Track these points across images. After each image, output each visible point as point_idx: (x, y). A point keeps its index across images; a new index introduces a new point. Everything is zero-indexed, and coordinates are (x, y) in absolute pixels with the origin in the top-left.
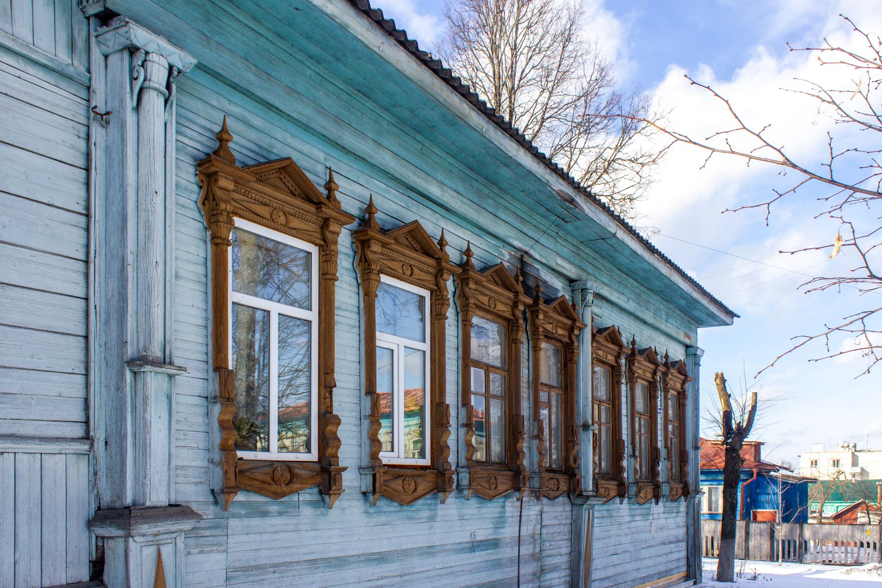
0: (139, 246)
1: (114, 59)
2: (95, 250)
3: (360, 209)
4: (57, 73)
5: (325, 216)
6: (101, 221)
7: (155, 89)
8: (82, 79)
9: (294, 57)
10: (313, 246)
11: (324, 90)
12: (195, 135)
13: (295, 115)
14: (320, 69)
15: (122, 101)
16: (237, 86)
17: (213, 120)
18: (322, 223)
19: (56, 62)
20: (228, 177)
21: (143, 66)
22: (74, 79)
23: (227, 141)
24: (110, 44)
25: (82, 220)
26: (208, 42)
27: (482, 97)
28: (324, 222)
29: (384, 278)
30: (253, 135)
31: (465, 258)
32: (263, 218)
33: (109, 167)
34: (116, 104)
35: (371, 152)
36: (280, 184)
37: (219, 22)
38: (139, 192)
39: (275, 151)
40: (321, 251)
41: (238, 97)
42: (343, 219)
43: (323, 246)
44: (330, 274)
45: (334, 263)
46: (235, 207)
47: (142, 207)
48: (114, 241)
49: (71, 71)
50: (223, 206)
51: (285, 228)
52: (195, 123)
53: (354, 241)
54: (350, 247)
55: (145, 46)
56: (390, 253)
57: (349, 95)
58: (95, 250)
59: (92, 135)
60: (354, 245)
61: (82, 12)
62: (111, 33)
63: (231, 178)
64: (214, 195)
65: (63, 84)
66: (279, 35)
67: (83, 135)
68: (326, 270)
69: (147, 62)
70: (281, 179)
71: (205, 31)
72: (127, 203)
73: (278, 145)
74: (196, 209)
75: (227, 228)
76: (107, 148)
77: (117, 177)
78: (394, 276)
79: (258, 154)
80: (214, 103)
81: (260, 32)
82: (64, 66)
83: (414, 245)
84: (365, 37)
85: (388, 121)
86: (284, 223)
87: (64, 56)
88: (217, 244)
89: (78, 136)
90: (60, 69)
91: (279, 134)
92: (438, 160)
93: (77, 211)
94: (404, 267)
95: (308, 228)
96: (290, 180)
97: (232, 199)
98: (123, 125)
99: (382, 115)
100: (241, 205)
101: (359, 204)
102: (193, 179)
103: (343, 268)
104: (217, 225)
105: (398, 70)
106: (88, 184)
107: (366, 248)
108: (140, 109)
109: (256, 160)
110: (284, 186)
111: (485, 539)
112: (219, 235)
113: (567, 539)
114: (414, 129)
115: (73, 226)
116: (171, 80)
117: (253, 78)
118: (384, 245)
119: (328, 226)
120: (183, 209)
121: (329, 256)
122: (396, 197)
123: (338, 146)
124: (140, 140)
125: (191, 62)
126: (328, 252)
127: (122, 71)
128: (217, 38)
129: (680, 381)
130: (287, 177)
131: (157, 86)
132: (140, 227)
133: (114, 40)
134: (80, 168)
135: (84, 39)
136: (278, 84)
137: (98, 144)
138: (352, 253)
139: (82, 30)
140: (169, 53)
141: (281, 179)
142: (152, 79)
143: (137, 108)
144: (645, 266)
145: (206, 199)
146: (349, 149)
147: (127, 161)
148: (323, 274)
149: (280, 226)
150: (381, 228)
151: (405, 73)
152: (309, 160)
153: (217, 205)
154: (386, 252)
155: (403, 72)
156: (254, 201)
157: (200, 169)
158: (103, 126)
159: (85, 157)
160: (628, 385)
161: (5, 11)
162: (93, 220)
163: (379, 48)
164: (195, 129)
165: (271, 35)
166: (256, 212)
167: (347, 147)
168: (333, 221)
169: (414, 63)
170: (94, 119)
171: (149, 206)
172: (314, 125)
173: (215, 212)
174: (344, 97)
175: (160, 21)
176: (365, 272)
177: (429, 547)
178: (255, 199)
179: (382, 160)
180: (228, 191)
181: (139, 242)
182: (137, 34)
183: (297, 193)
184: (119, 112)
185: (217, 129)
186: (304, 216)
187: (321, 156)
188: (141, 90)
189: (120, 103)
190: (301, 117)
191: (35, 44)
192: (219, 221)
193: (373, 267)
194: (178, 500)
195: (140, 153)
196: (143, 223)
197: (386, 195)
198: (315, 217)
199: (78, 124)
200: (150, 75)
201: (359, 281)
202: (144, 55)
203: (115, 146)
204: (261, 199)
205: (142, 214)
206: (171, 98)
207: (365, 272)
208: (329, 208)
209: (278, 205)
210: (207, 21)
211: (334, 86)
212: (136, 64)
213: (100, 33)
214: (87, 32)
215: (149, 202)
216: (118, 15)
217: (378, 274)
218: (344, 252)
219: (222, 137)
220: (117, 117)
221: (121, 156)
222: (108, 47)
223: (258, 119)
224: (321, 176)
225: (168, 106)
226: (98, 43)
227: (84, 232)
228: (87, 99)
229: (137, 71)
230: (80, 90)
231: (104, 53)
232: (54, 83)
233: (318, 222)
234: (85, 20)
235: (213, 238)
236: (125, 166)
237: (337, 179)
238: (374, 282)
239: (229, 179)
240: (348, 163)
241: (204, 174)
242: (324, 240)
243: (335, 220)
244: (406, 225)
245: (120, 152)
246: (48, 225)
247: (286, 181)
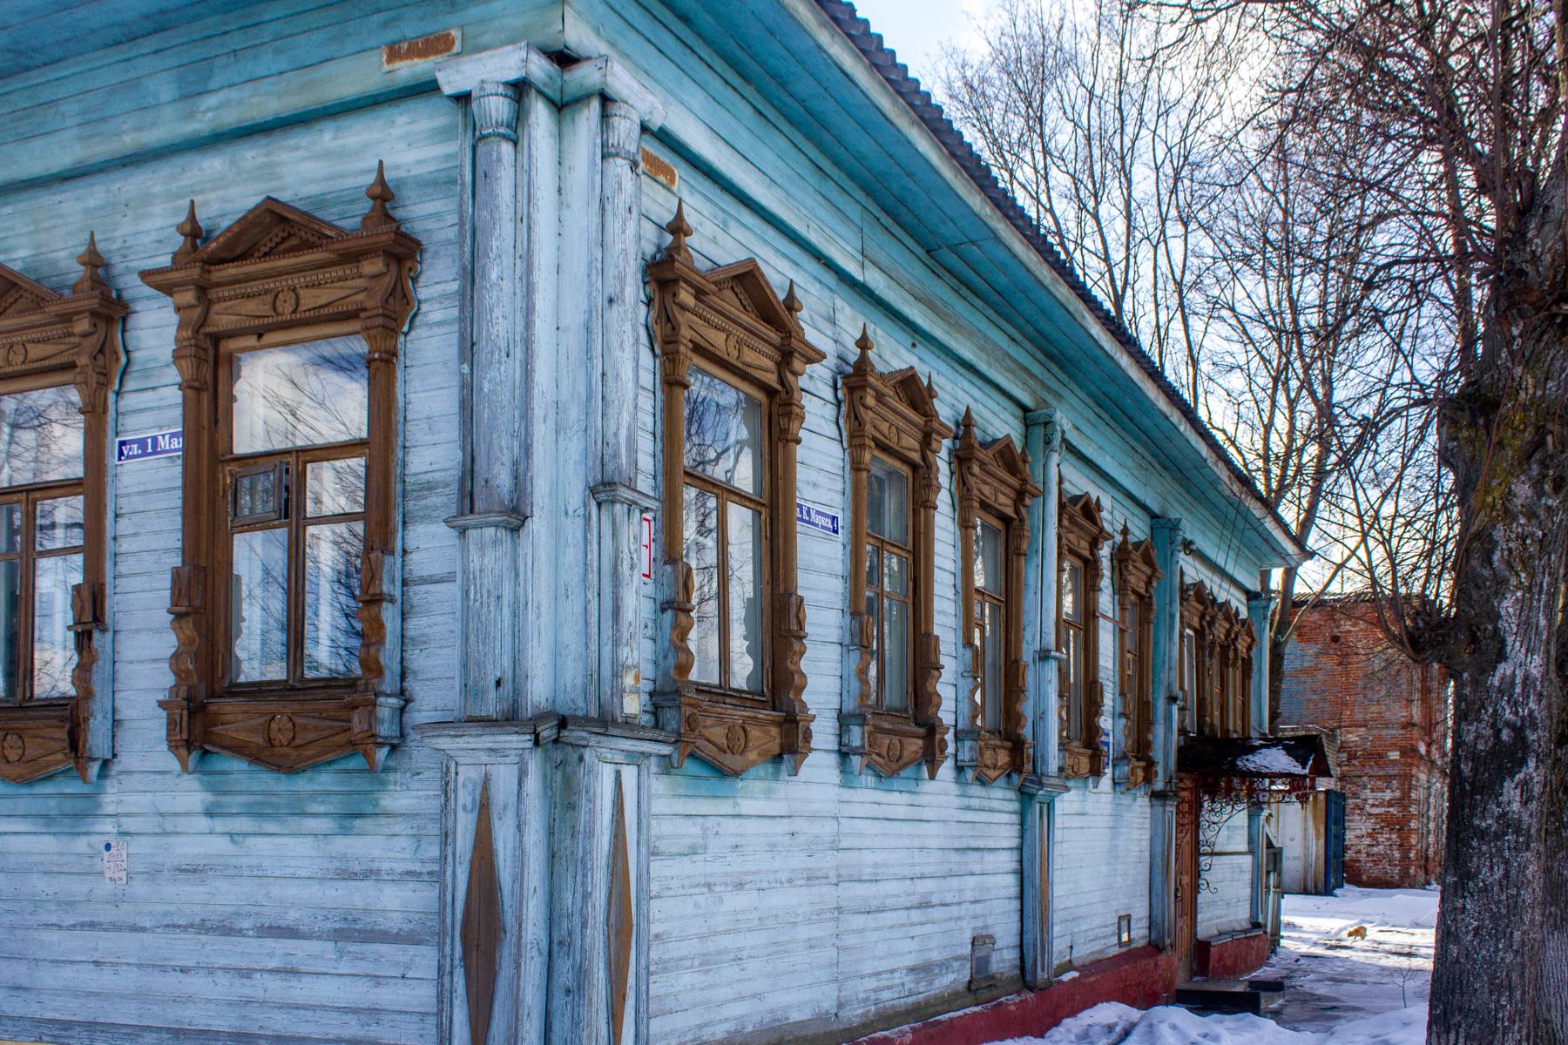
27: (1171, 378)
31: (669, 238)
113: (1014, 812)
129: (1145, 578)
144: (1001, 254)
194: (832, 731)
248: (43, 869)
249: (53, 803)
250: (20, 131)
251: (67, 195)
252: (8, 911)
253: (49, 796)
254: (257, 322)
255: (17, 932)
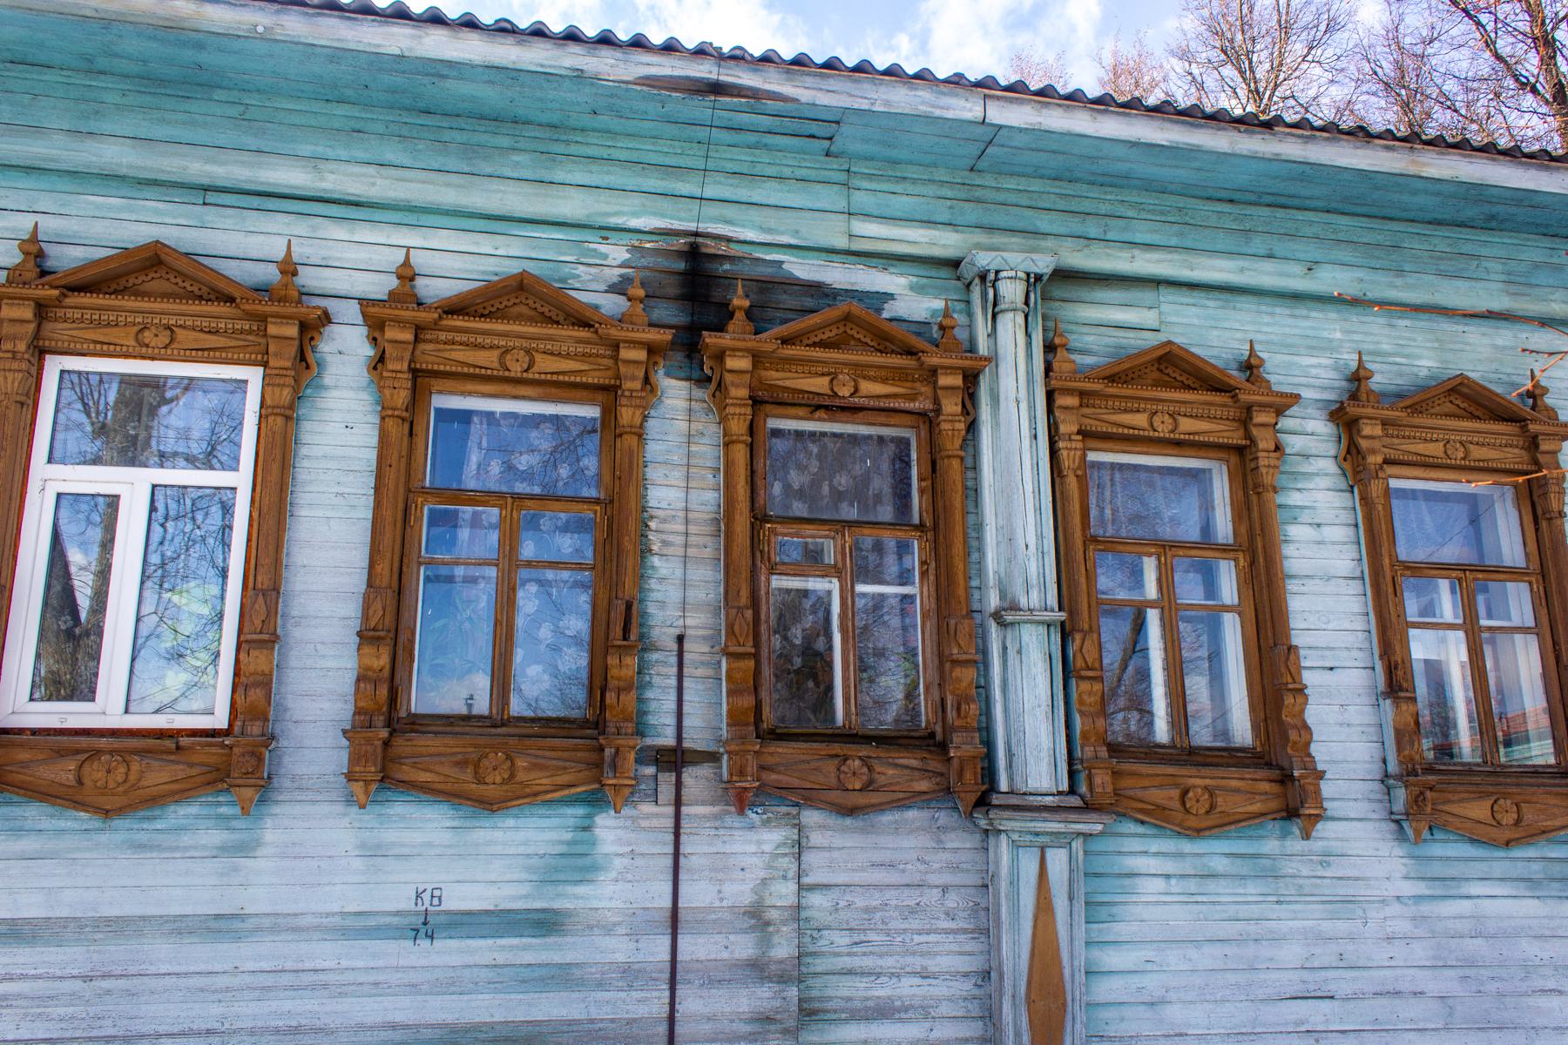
78: (126, 356)
92: (297, 119)
111: (492, 908)
119: (1251, 418)
160: (1356, 490)
177: (218, 917)
219: (1358, 378)
248: (1532, 933)
249: (1536, 867)
250: (1442, 268)
251: (1472, 329)
252: (1493, 978)
253: (1529, 860)
254: (1120, 430)
255: (1508, 999)
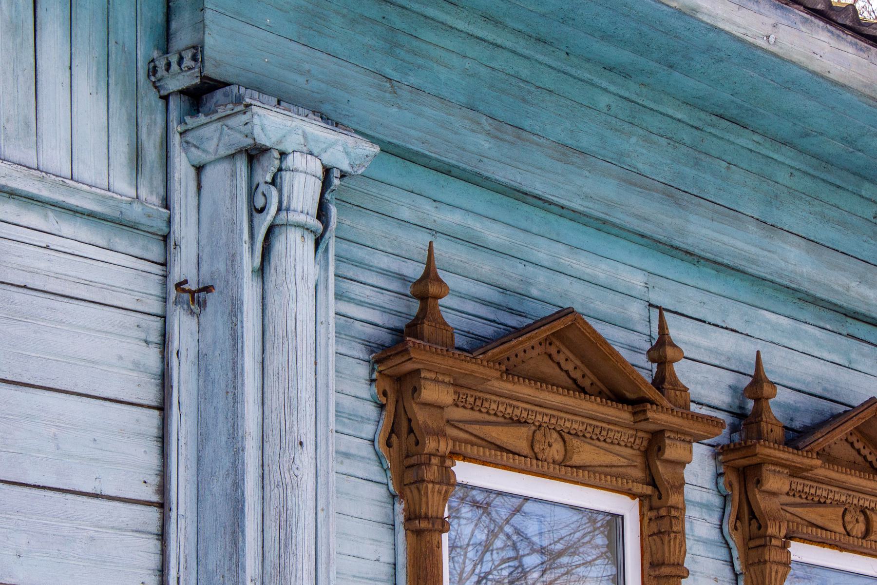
0: (267, 562)
1: (214, 175)
2: (178, 578)
3: (733, 388)
4: (112, 222)
5: (652, 427)
6: (188, 514)
7: (298, 226)
8: (154, 224)
9: (571, 75)
10: (626, 499)
11: (641, 131)
12: (368, 291)
13: (576, 204)
14: (631, 89)
15: (233, 259)
16: (452, 169)
17: (404, 254)
18: (645, 443)
19: (112, 203)
20: (441, 378)
21: (273, 183)
22: (141, 227)
23: (437, 297)
24: (211, 146)
25: (152, 515)
26: (395, 93)
28: (650, 442)
29: (799, 551)
30: (486, 266)
32: (514, 453)
33: (203, 397)
34: (221, 266)
35: (753, 250)
36: (548, 369)
37: (415, 43)
38: (267, 446)
39: (534, 292)
40: (646, 509)
41: (453, 191)
42: (696, 428)
43: (649, 497)
44: (669, 565)
45: (679, 536)
46: (455, 440)
47: (273, 477)
48: (215, 558)
49: (136, 212)
50: (430, 445)
51: (563, 469)
52: (368, 267)
53: (722, 471)
54: (714, 487)
55: (280, 142)
56: (810, 488)
57: (697, 128)
58: (178, 578)
59: (173, 329)
60: (721, 480)
61: (156, 87)
62: (213, 127)
63: (447, 380)
64: (410, 420)
65: (121, 242)
66: (538, 40)
67: (155, 337)
68: (659, 556)
69: (284, 173)
70: (550, 356)
71: (389, 71)
72: (243, 473)
73: (542, 277)
74: (373, 456)
75: (439, 492)
76: (201, 357)
77: (221, 419)
78: (822, 543)
79: (498, 307)
80: (406, 214)
81: (499, 41)
82: (124, 205)
83: (870, 458)
84: (734, 23)
85: (792, 168)
86: (559, 457)
87: (123, 186)
88: (419, 533)
89: (146, 342)
90: (117, 214)
91: (543, 251)
93: (142, 498)
94: (848, 518)
95: (615, 460)
96: (571, 356)
97: (448, 421)
98: (235, 311)
99: (775, 156)
100: (467, 432)
101: (729, 378)
102: (364, 390)
103: (699, 540)
104: (419, 490)
105: (814, 73)
106: (163, 438)
107: (751, 486)
108: (267, 270)
109: (494, 321)
110: (558, 370)
112: (423, 511)
114: (854, 174)
115: (137, 531)
116: (328, 196)
117: (484, 143)
118: (795, 472)
119: (661, 449)
120: (346, 461)
121: (666, 521)
122: (819, 344)
123: (674, 252)
124: (268, 334)
125: (367, 153)
126: (663, 512)
127: (233, 197)
128: (412, 79)
130: (564, 349)
131: (302, 218)
132: (267, 522)
133: (220, 139)
134: (149, 407)
135: (158, 140)
136: (538, 144)
137: (183, 353)
138: (716, 501)
139: (155, 124)
140: (324, 146)
141: (550, 356)
142: (292, 208)
143: (262, 271)
145: (392, 431)
146: (703, 254)
147: (243, 384)
148: (652, 565)
149: (552, 466)
150: (785, 427)
151: (831, 76)
152: (611, 295)
153: (417, 443)
154: (800, 488)
155: (828, 75)
156: (493, 418)
157: (380, 369)
158: (192, 313)
159: (158, 388)
161: (27, 125)
162: (173, 514)
163: (768, 37)
164: (370, 281)
165: (522, 42)
166: (498, 443)
167: (696, 251)
168: (672, 436)
169: (851, 50)
170: (176, 303)
171: (287, 475)
172: (621, 216)
173: (413, 460)
174: (686, 135)
175: (301, 73)
176: (752, 544)
178: (495, 414)
179: (783, 264)
180: (441, 407)
181: (267, 555)
182: (265, 122)
183: (586, 383)
184: (227, 282)
185: (415, 271)
186: (604, 433)
187: (637, 280)
188: (271, 230)
189: (230, 264)
190: (591, 205)
191: (75, 176)
192: (423, 481)
193: (772, 530)
195: (267, 363)
196: (273, 512)
197: (793, 344)
198: (631, 432)
199: (146, 317)
200: (289, 197)
201: (738, 567)
202: (277, 162)
203: (217, 353)
204: (509, 410)
205: (273, 494)
206: (327, 235)
207: (752, 544)
208: (663, 409)
209: (546, 419)
210: (392, 46)
211: (660, 117)
212: (261, 181)
213: (189, 127)
214: (164, 125)
215: (286, 466)
216: (226, 84)
217: (785, 546)
218: (698, 499)
220: (221, 293)
221: (230, 375)
222: (204, 151)
223: (497, 227)
224: (639, 329)
225: (321, 250)
226: (185, 145)
227: (156, 542)
228: (161, 260)
229: (264, 195)
230: (150, 246)
231: (195, 164)
232: (104, 244)
233: (638, 441)
234: (161, 103)
235: (409, 519)
236: (240, 396)
237: (679, 331)
238: (774, 567)
239: (443, 382)
240: (701, 284)
241: (389, 376)
242: (652, 482)
243: (677, 432)
244: (852, 410)
245: (230, 365)
246: (92, 539)
247: (561, 358)
